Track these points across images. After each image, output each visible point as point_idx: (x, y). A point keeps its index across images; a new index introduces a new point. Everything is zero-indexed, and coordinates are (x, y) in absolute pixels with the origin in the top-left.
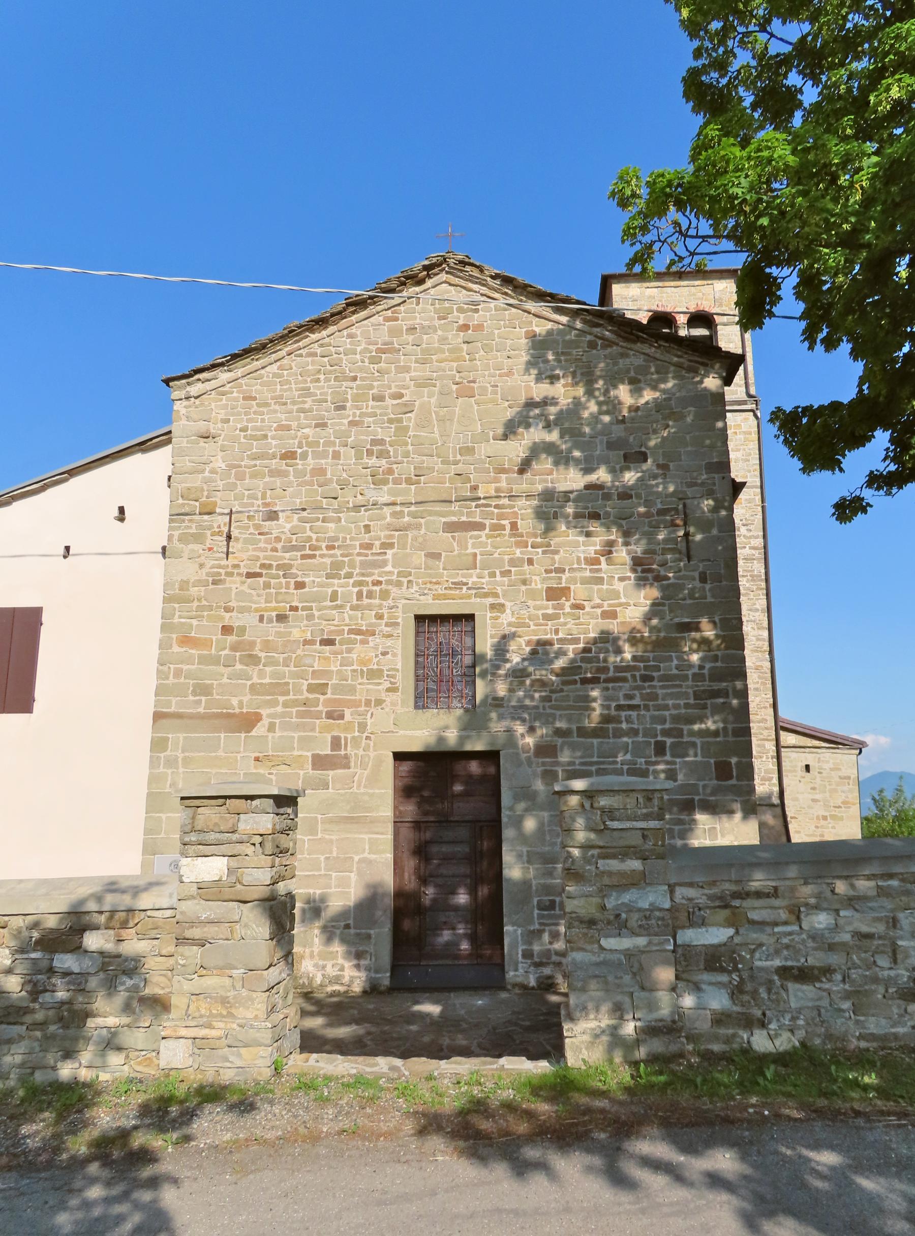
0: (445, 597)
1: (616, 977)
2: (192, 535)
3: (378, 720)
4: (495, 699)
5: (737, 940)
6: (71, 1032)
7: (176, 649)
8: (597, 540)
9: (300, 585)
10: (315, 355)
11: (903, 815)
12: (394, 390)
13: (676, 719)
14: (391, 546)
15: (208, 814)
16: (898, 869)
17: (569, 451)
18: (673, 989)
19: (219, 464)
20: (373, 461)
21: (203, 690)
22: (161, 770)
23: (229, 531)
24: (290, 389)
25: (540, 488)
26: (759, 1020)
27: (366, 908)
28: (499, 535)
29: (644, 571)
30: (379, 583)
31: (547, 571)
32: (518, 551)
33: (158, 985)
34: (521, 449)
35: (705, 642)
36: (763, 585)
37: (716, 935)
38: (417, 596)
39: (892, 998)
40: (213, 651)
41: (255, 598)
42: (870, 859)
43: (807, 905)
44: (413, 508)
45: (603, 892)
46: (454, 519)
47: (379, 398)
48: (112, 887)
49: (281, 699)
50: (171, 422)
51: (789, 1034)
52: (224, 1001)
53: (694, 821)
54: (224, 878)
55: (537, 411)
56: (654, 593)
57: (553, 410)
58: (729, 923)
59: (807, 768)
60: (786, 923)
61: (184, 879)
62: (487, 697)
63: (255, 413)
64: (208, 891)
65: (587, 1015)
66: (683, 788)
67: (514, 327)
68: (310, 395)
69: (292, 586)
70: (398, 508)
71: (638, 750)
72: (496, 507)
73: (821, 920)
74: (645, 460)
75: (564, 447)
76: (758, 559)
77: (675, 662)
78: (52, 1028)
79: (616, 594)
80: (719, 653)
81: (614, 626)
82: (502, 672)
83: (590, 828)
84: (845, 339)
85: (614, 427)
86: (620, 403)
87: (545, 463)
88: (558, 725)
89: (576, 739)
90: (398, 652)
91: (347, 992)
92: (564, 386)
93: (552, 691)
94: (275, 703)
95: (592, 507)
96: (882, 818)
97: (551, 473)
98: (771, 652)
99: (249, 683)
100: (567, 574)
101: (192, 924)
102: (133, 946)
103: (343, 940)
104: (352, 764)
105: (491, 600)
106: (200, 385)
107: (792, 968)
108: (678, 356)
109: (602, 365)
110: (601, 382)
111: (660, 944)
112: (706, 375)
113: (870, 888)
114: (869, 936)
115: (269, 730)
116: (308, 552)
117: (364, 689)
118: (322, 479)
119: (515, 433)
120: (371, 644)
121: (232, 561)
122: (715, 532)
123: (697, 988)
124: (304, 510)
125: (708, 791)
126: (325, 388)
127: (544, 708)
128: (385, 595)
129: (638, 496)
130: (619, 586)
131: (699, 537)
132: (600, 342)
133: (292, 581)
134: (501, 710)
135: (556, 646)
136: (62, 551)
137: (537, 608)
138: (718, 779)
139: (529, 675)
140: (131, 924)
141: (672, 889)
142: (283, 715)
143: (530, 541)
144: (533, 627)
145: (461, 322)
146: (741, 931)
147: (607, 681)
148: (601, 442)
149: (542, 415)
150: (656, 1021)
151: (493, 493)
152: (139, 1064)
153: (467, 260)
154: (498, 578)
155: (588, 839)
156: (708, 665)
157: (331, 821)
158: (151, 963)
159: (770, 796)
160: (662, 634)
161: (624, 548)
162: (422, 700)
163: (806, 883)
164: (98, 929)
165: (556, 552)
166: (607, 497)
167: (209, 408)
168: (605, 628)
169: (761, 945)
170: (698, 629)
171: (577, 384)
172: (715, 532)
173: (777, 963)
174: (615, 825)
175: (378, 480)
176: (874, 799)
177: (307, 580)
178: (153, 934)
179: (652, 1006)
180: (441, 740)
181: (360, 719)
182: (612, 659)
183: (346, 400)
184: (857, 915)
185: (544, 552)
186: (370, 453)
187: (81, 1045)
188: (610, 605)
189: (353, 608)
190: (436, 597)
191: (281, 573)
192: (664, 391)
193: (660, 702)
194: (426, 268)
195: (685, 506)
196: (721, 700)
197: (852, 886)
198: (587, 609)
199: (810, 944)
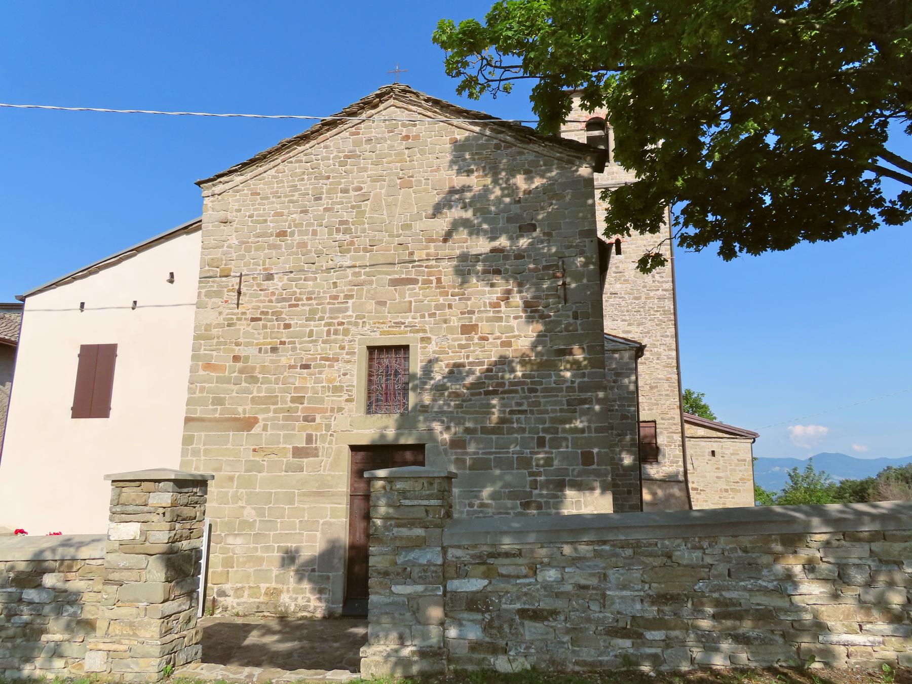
0: (389, 333)
1: (400, 614)
2: (214, 292)
3: (339, 422)
4: (423, 406)
5: (489, 589)
6: (31, 643)
7: (201, 372)
8: (499, 289)
9: (287, 326)
10: (301, 161)
11: (812, 487)
12: (356, 184)
13: (553, 420)
14: (351, 297)
15: (130, 493)
16: (610, 537)
17: (480, 224)
18: (442, 624)
19: (234, 241)
20: (340, 236)
21: (218, 401)
22: (189, 458)
23: (240, 288)
24: (283, 187)
25: (458, 252)
26: (502, 648)
27: (327, 556)
28: (428, 287)
29: (532, 310)
30: (342, 323)
31: (462, 313)
32: (441, 299)
33: (89, 612)
34: (445, 225)
35: (576, 363)
36: (672, 317)
37: (475, 584)
38: (368, 332)
39: (600, 634)
40: (227, 374)
41: (256, 336)
42: (589, 529)
43: (542, 563)
44: (368, 269)
45: (397, 551)
46: (397, 276)
47: (345, 191)
48: (67, 543)
49: (272, 407)
50: (201, 213)
51: (523, 659)
52: (131, 625)
53: (565, 495)
54: (138, 538)
55: (457, 196)
56: (540, 327)
57: (468, 195)
58: (485, 576)
59: (713, 453)
60: (526, 577)
61: (111, 538)
62: (416, 405)
63: (259, 204)
64: (126, 547)
65: (379, 641)
66: (559, 471)
67: (441, 135)
68: (297, 190)
69: (282, 327)
70: (357, 270)
71: (524, 444)
72: (427, 267)
73: (552, 575)
74: (535, 230)
75: (476, 222)
76: (669, 298)
77: (554, 378)
78: (19, 641)
79: (512, 329)
80: (586, 371)
81: (509, 352)
82: (427, 387)
83: (389, 505)
84: (772, 131)
85: (512, 207)
86: (517, 188)
87: (463, 234)
88: (468, 425)
89: (480, 435)
90: (354, 374)
91: (311, 617)
92: (477, 177)
93: (463, 401)
94: (268, 410)
95: (496, 265)
96: (796, 489)
97: (466, 241)
98: (678, 368)
99: (251, 396)
100: (476, 315)
101: (115, 569)
102: (76, 584)
103: (311, 580)
104: (320, 454)
105: (421, 335)
106: (221, 186)
107: (528, 610)
108: (560, 153)
109: (505, 161)
110: (503, 174)
111: (432, 591)
112: (580, 166)
113: (588, 551)
114: (585, 587)
115: (263, 430)
116: (293, 302)
117: (330, 400)
118: (304, 250)
119: (441, 213)
120: (336, 368)
121: (241, 310)
122: (585, 281)
123: (460, 624)
124: (291, 272)
125: (575, 473)
126: (307, 185)
127: (457, 413)
128: (346, 332)
129: (529, 256)
130: (514, 323)
131: (573, 285)
132: (503, 144)
133: (282, 323)
134: (426, 415)
135: (467, 368)
136: (131, 304)
137: (454, 340)
138: (583, 464)
139: (447, 389)
140: (75, 569)
141: (444, 550)
142: (273, 419)
143: (450, 291)
144: (451, 354)
145: (404, 134)
146: (493, 582)
147: (504, 392)
148: (503, 217)
149: (460, 199)
150: (428, 647)
151: (424, 257)
152: (74, 668)
153: (408, 89)
154: (427, 319)
155: (388, 513)
156: (578, 381)
157: (305, 494)
158: (86, 597)
159: (677, 475)
160: (545, 358)
161: (518, 295)
162: (372, 407)
163: (542, 547)
164: (53, 572)
165: (469, 299)
166: (506, 258)
167: (231, 203)
168: (503, 354)
169: (507, 592)
170: (571, 353)
171: (486, 175)
172: (585, 281)
173: (518, 606)
174: (407, 502)
175: (343, 250)
176: (790, 475)
177: (292, 322)
178: (90, 576)
179: (425, 636)
180: (383, 436)
181: (326, 421)
182: (507, 376)
183: (322, 193)
184: (578, 571)
185: (460, 299)
186: (338, 230)
187: (36, 653)
188: (507, 337)
189: (324, 342)
190: (382, 333)
191: (275, 318)
192: (550, 179)
193: (542, 408)
194: (378, 96)
195: (563, 262)
196: (587, 406)
197: (576, 550)
198: (491, 340)
199: (543, 592)
